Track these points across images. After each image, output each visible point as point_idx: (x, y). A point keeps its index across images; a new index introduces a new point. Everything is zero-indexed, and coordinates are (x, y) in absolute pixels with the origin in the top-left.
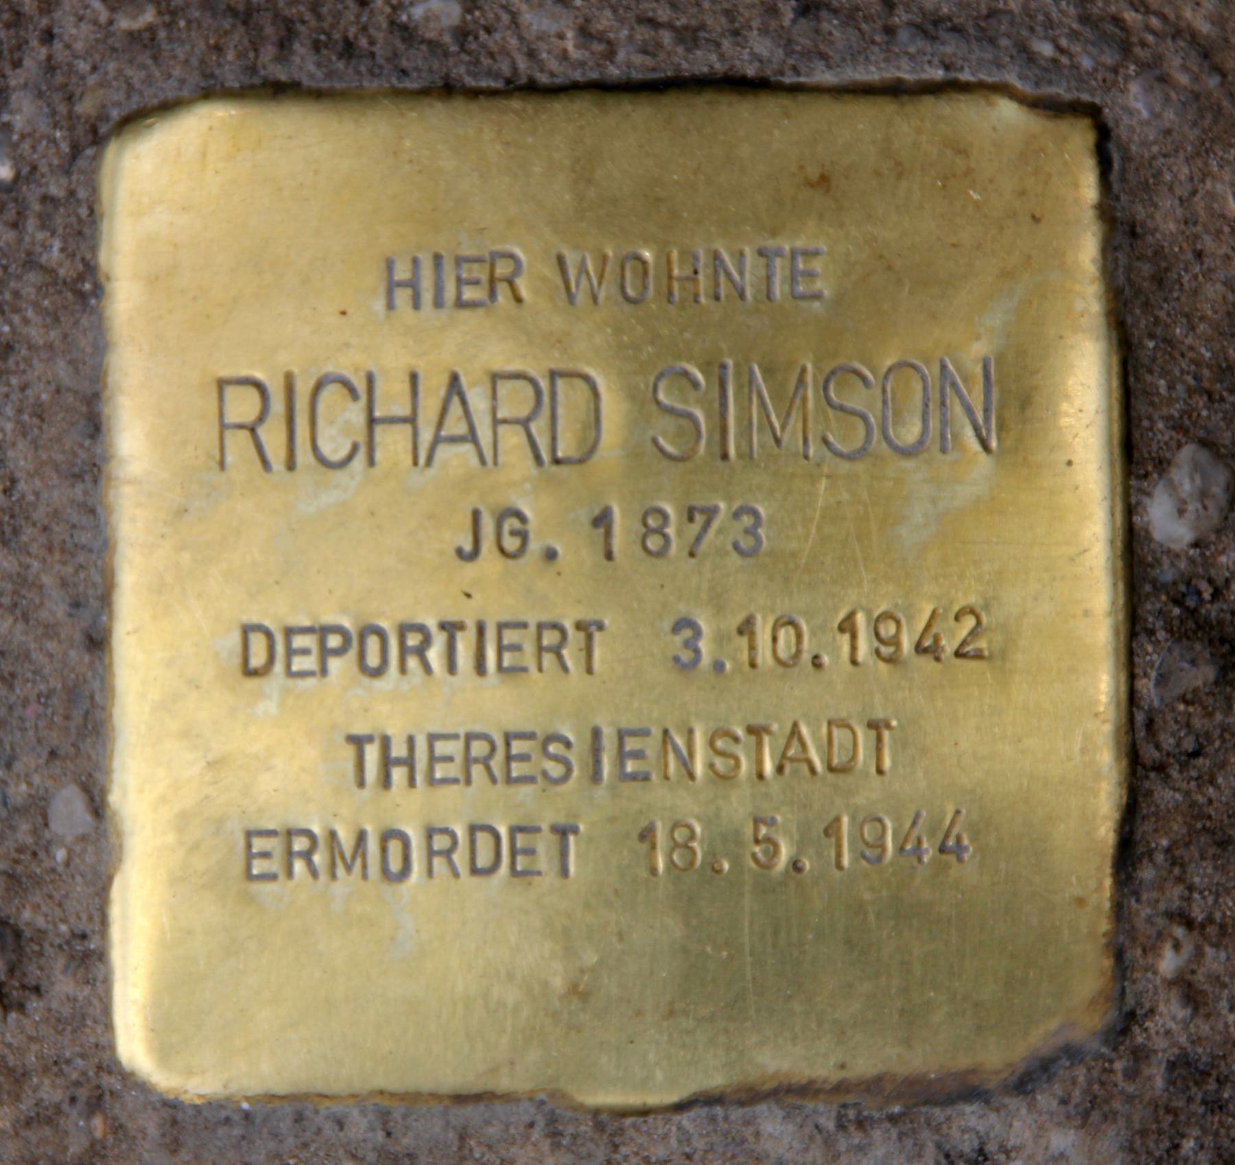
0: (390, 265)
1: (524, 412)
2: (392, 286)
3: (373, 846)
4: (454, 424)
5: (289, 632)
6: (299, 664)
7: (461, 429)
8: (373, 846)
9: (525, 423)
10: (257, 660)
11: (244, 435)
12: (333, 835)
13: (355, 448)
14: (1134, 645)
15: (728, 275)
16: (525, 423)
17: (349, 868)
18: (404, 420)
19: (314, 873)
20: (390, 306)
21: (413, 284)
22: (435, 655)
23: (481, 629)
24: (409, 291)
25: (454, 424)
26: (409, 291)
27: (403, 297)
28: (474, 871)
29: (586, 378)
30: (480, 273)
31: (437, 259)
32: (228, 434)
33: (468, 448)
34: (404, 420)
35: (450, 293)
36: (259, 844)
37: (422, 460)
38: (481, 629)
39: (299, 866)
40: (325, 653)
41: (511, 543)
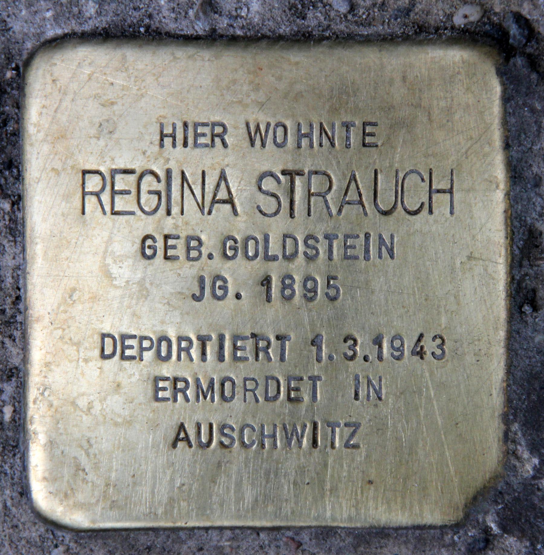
0: (162, 126)
1: (97, 189)
2: (162, 136)
3: (217, 387)
4: (352, 195)
5: (124, 337)
6: (128, 352)
7: (356, 198)
8: (217, 387)
9: (97, 195)
10: (108, 351)
11: (94, 199)
12: (197, 381)
13: (423, 204)
14: (533, 295)
15: (261, 134)
16: (97, 195)
17: (205, 397)
18: (313, 195)
19: (187, 400)
20: (162, 145)
21: (173, 136)
22: (195, 353)
23: (221, 338)
24: (171, 139)
25: (352, 195)
26: (171, 139)
27: (168, 141)
28: (267, 399)
29: (329, 176)
30: (207, 130)
31: (185, 125)
32: (87, 198)
33: (228, 207)
34: (313, 195)
35: (190, 141)
36: (161, 384)
37: (206, 210)
38: (221, 338)
39: (180, 396)
40: (142, 349)
41: (219, 293)
